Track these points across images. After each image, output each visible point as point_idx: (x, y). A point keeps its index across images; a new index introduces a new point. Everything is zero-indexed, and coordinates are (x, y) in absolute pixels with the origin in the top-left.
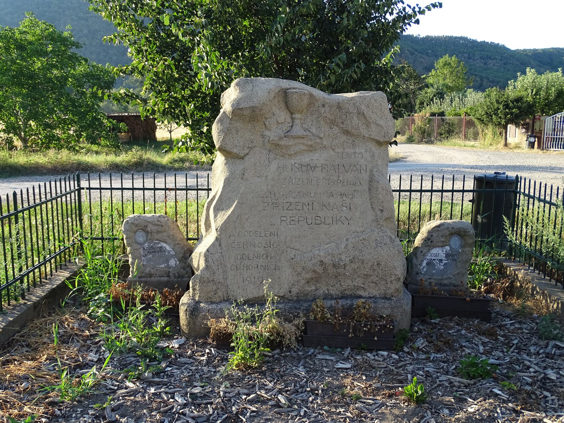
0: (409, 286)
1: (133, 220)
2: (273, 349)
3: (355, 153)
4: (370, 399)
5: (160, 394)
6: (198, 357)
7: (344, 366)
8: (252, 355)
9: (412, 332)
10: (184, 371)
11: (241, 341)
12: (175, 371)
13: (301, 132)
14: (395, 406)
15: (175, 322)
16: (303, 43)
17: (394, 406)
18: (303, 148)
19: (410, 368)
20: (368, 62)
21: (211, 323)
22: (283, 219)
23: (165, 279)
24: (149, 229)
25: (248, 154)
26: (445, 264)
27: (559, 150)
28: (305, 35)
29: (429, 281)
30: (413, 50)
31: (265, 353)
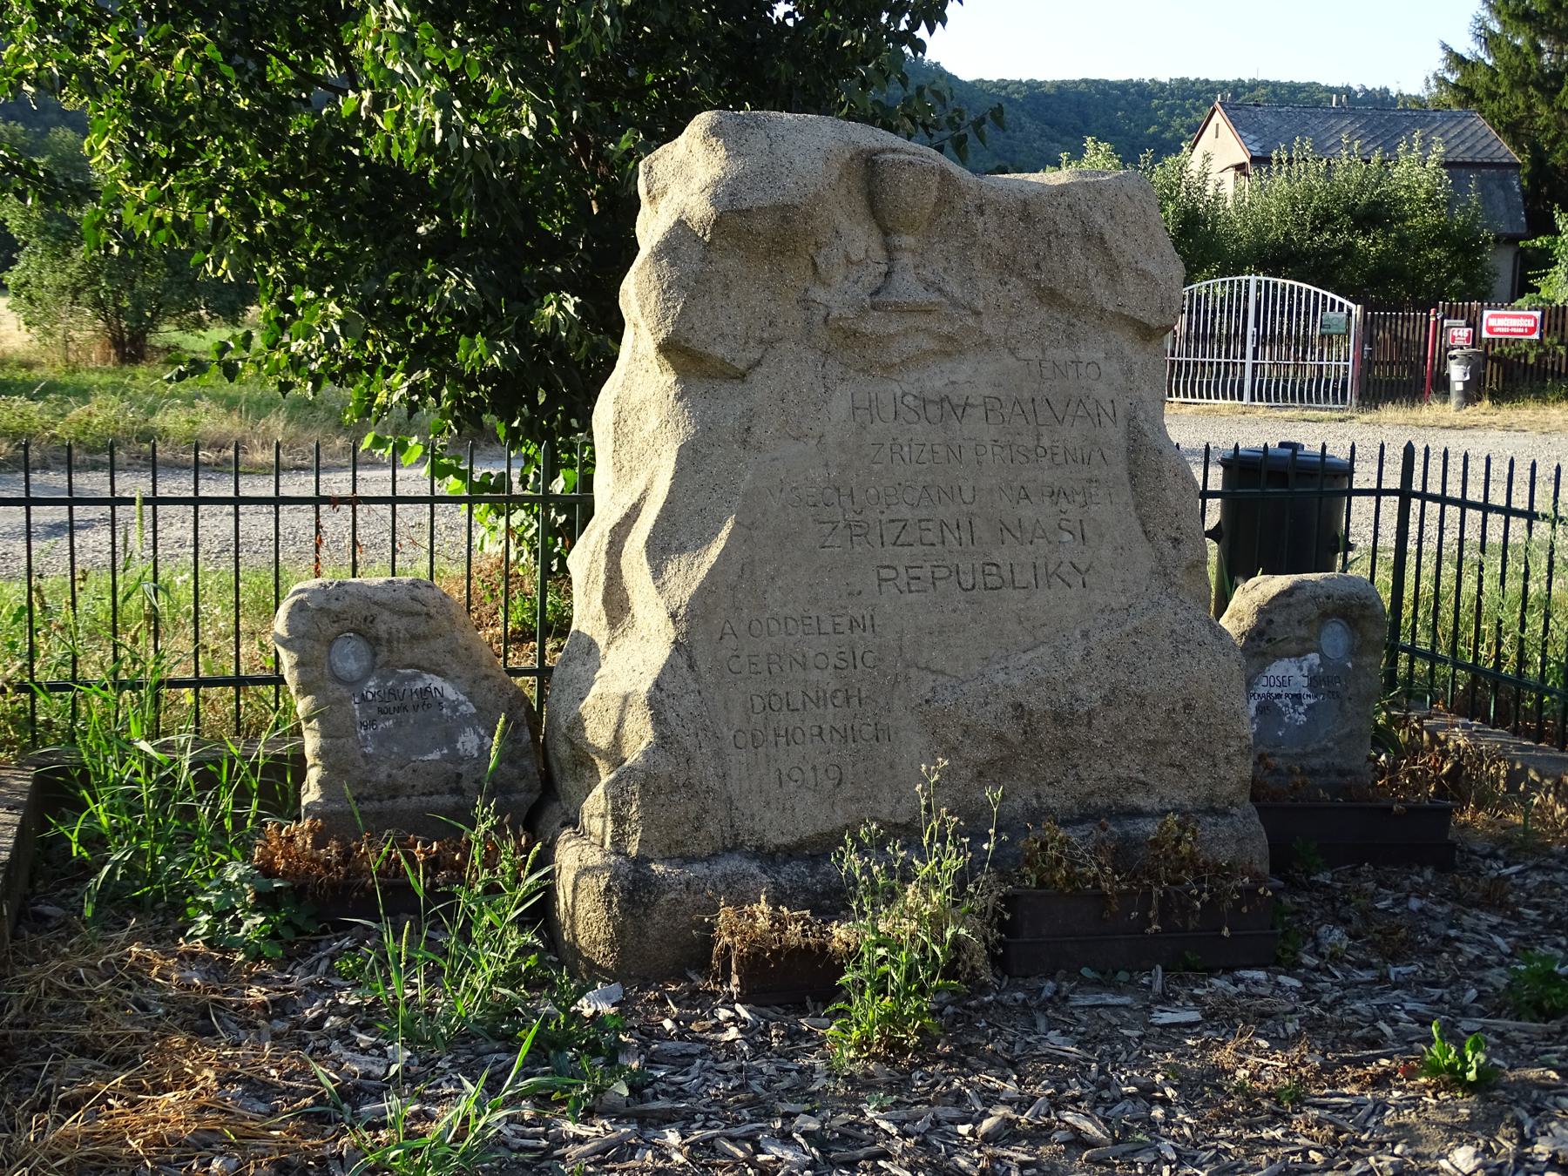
1: (322, 598)
3: (1077, 362)
13: (922, 296)
18: (929, 344)
22: (885, 573)
24: (382, 629)
25: (759, 363)
26: (1310, 707)
27: (1197, 400)
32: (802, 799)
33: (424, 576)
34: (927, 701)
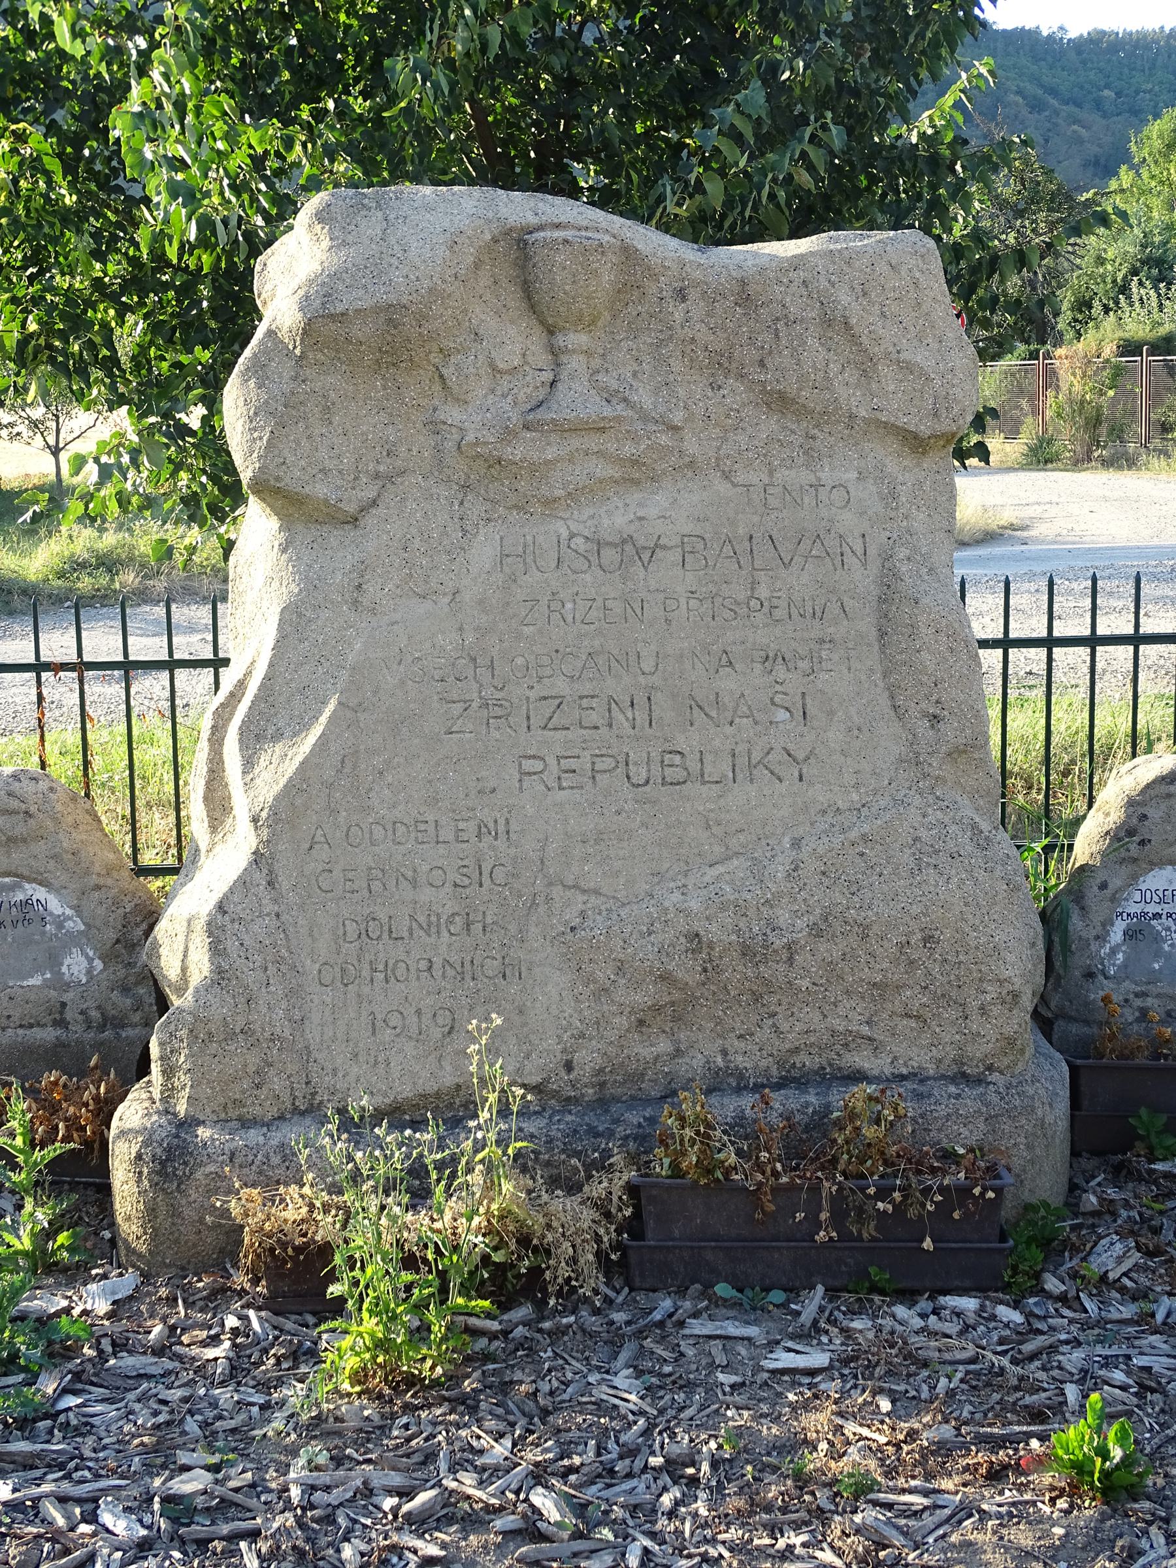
0: (1059, 1026)
2: (504, 1305)
3: (817, 486)
4: (911, 1491)
5: (34, 1507)
6: (195, 1351)
7: (800, 1361)
8: (421, 1333)
9: (1076, 1215)
10: (137, 1407)
11: (369, 1270)
12: (99, 1408)
13: (593, 408)
14: (1017, 1514)
15: (93, 1210)
16: (588, 52)
17: (1011, 1515)
19: (1073, 1359)
20: (860, 122)
21: (246, 1206)
22: (528, 765)
23: (48, 1035)
25: (374, 503)
28: (597, 22)
29: (1138, 1002)
30: (1040, 92)
31: (473, 1321)
32: (401, 1051)
33: (33, 764)
34: (573, 929)
